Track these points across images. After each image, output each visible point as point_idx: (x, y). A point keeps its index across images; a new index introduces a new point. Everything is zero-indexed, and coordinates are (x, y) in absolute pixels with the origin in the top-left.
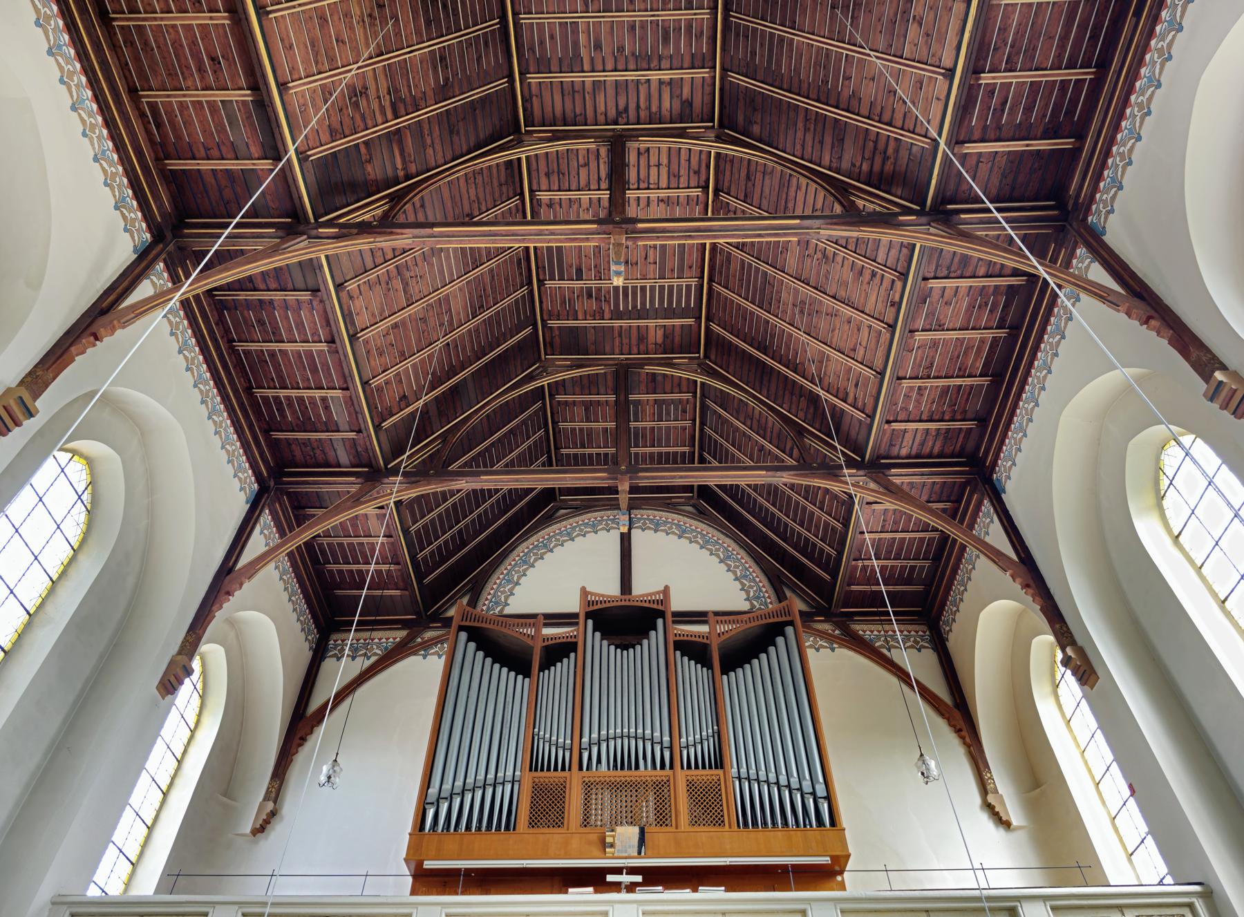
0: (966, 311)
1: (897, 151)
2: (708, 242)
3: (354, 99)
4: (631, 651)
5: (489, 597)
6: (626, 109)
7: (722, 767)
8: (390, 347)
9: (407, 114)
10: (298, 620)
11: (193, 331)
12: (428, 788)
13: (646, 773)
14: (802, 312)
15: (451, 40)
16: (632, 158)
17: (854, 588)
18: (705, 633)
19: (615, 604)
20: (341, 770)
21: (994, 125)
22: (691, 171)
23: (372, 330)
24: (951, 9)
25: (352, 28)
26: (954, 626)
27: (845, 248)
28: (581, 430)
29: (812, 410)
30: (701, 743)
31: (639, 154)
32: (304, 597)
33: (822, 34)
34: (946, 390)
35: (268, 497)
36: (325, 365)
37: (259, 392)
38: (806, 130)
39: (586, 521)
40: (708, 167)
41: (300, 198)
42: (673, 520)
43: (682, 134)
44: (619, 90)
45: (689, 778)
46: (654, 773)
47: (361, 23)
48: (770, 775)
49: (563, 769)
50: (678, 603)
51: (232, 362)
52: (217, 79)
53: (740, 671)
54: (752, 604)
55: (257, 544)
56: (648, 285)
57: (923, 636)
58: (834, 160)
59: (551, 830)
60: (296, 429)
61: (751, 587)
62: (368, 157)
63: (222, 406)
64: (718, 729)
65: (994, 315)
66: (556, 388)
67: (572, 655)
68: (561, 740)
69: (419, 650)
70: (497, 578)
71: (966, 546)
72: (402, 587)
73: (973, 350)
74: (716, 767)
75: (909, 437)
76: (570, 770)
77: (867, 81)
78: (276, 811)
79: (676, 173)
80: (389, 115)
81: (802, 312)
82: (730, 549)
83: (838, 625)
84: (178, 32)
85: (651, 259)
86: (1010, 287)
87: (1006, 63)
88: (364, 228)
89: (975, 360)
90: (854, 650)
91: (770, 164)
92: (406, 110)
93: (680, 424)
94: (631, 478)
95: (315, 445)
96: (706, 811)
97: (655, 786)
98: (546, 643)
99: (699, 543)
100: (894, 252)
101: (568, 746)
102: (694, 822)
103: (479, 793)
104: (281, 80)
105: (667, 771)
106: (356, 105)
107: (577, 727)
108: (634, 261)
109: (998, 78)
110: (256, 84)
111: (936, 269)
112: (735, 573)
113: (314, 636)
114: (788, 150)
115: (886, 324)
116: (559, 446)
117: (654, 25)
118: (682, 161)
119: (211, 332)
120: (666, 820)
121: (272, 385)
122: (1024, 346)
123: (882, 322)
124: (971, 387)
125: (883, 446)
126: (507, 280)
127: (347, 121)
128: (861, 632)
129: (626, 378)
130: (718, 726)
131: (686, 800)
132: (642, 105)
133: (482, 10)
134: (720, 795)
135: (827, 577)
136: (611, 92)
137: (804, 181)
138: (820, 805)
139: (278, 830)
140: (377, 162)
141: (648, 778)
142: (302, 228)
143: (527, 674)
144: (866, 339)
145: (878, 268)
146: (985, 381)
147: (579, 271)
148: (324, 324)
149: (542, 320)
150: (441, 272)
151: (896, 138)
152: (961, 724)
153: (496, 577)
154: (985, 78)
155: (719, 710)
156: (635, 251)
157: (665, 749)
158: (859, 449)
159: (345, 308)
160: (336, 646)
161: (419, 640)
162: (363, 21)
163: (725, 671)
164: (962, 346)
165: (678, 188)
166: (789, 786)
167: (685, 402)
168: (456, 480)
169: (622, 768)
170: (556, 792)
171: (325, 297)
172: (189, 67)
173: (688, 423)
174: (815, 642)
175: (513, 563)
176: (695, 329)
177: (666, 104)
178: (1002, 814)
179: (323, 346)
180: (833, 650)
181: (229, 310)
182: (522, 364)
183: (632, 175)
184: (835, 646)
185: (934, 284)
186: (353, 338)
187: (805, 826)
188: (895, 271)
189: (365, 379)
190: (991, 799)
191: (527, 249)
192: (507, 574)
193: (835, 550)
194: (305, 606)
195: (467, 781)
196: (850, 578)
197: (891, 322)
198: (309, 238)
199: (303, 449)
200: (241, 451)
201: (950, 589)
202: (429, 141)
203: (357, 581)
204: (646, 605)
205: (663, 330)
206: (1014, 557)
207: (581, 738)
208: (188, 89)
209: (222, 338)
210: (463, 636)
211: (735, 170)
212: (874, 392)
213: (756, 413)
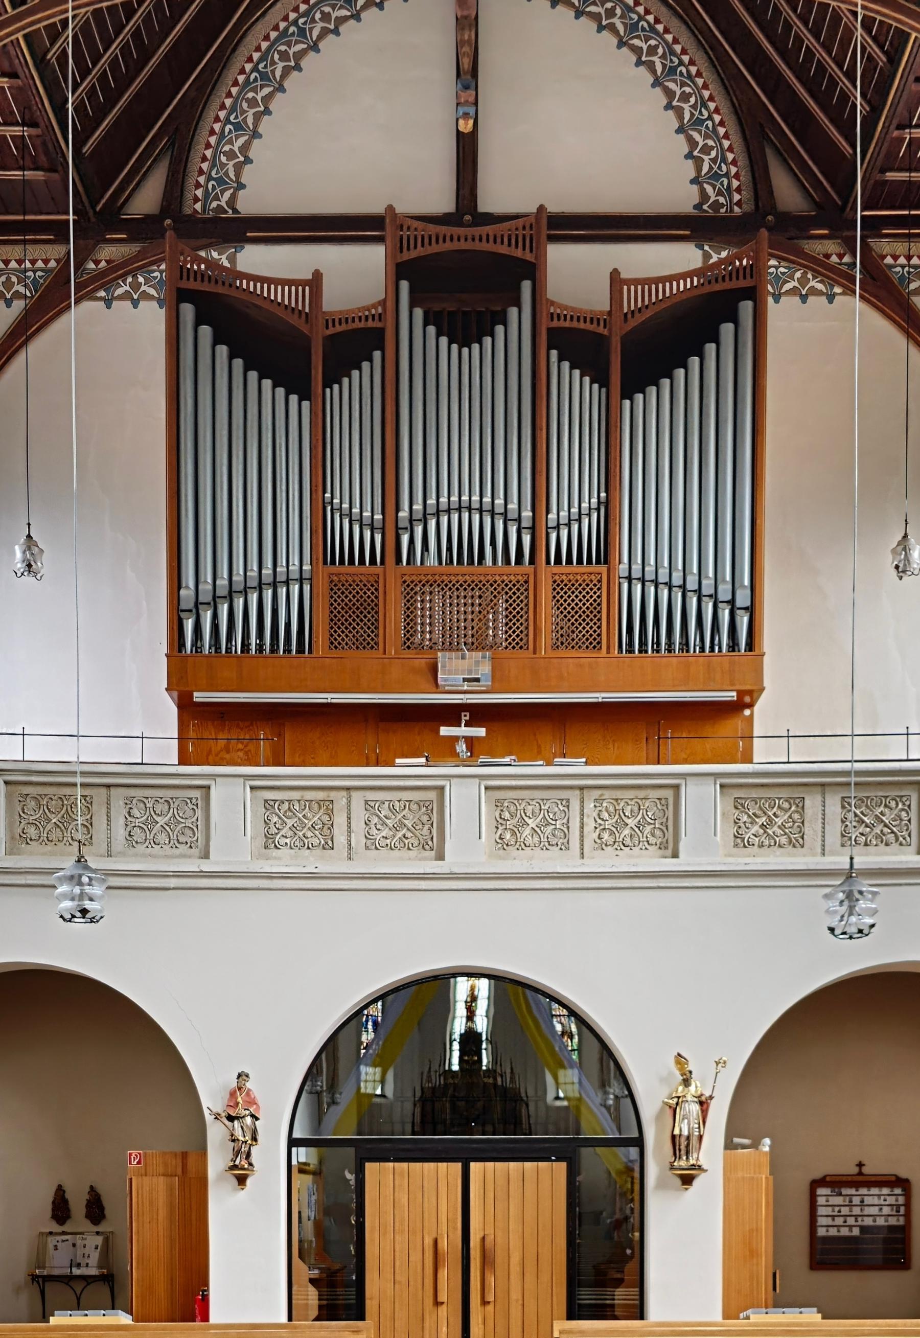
4: (476, 347)
7: (606, 562)
12: (179, 588)
17: (891, 176)
18: (602, 313)
20: (42, 551)
30: (579, 521)
45: (557, 577)
46: (507, 569)
64: (607, 496)
68: (367, 514)
74: (598, 562)
98: (331, 331)
130: (607, 491)
134: (599, 597)
138: (738, 619)
141: (497, 578)
153: (212, 115)
157: (524, 531)
163: (627, 394)
174: (803, 281)
180: (831, 298)
184: (837, 290)
192: (233, 109)
193: (884, 53)
196: (888, 155)
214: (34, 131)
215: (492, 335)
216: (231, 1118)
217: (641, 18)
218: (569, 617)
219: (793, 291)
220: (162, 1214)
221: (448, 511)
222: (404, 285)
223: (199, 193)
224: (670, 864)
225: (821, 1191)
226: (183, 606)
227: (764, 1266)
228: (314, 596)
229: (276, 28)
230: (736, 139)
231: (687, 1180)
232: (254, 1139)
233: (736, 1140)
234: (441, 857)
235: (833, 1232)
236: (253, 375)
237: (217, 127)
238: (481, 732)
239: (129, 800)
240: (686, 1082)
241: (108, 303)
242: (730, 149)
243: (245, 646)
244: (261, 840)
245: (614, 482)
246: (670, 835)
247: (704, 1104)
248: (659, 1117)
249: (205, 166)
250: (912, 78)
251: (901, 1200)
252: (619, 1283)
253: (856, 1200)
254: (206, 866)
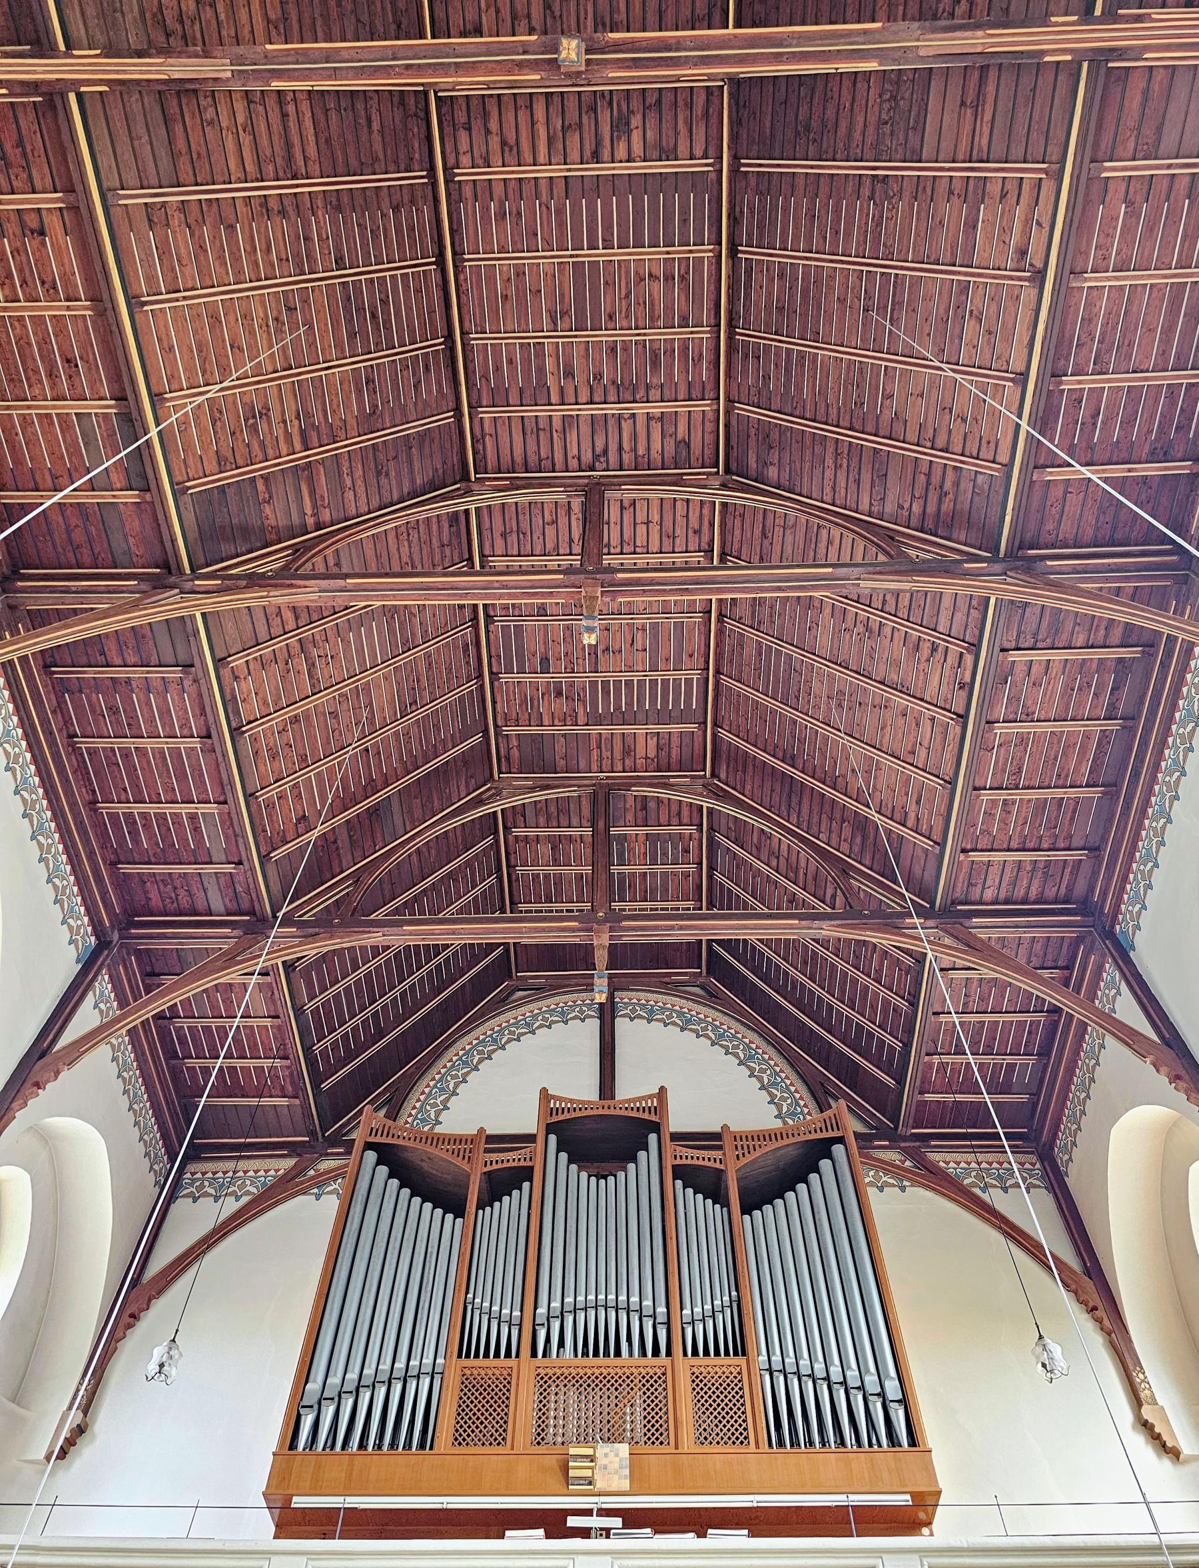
0: (1062, 695)
1: (957, 484)
2: (714, 598)
3: (251, 421)
4: (611, 1179)
5: (414, 1112)
6: (605, 452)
7: (744, 1354)
8: (287, 749)
9: (321, 446)
10: (141, 1139)
11: (21, 720)
12: (307, 1382)
13: (631, 1362)
14: (840, 706)
15: (382, 358)
16: (611, 512)
17: (929, 1097)
20: (181, 1355)
21: (1084, 445)
22: (690, 531)
23: (263, 723)
24: (1018, 297)
25: (252, 333)
26: (1076, 1153)
27: (895, 616)
28: (547, 876)
29: (858, 840)
31: (622, 508)
32: (152, 1106)
33: (853, 344)
34: (1041, 805)
35: (108, 956)
36: (196, 769)
38: (837, 467)
39: (553, 1007)
40: (712, 525)
41: (173, 541)
42: (673, 1006)
43: (678, 481)
44: (596, 426)
45: (695, 1369)
46: (643, 1362)
47: (264, 328)
48: (816, 1366)
49: (508, 1354)
50: (678, 1121)
51: (71, 766)
52: (72, 386)
53: (768, 1208)
54: (785, 1123)
55: (86, 1018)
56: (635, 679)
57: (1032, 1170)
58: (875, 503)
59: (487, 1450)
60: (153, 860)
61: (784, 1099)
62: (267, 496)
63: (53, 825)
65: (1101, 700)
66: (516, 815)
67: (526, 1185)
69: (311, 1187)
70: (424, 1086)
71: (1086, 1025)
72: (291, 1094)
73: (1075, 749)
75: (994, 872)
76: (517, 1356)
77: (914, 397)
78: (87, 1426)
79: (671, 534)
80: (298, 445)
81: (840, 706)
82: (754, 1046)
83: (909, 1153)
84: (25, 326)
85: (638, 645)
86: (1120, 660)
87: (1095, 364)
88: (255, 581)
89: (1079, 763)
90: (934, 1189)
91: (792, 514)
92: (319, 441)
93: (681, 868)
94: (611, 929)
95: (178, 883)
96: (720, 1422)
97: (644, 1381)
98: (489, 1168)
99: (709, 1038)
100: (960, 617)
101: (515, 1321)
102: (703, 1439)
103: (381, 1391)
104: (155, 390)
105: (663, 1359)
106: (254, 429)
107: (530, 1292)
108: (617, 648)
109: (1087, 383)
110: (123, 395)
111: (1018, 636)
112: (760, 1079)
114: (814, 496)
115: (954, 713)
116: (516, 899)
117: (640, 347)
118: (678, 518)
119: (44, 722)
120: (661, 1434)
121: (123, 798)
122: (1144, 742)
123: (950, 711)
124: (1077, 801)
125: (958, 890)
126: (449, 671)
127: (241, 451)
128: (942, 1164)
129: (607, 802)
130: (737, 1290)
131: (690, 1405)
132: (626, 446)
133: (422, 324)
135: (890, 1082)
136: (585, 429)
137: (836, 532)
139: (86, 1454)
140: (279, 504)
141: (634, 1370)
142: (172, 579)
143: (459, 1213)
144: (928, 736)
145: (939, 638)
146: (1095, 793)
147: (545, 660)
148: (198, 713)
149: (496, 726)
150: (360, 651)
151: (955, 468)
152: (1095, 1299)
154: (1068, 383)
155: (739, 1267)
156: (618, 635)
158: (925, 891)
159: (228, 691)
160: (194, 1181)
161: (312, 1172)
162: (267, 326)
163: (747, 1210)
164: (1059, 741)
165: (674, 552)
166: (844, 1383)
167: (687, 837)
168: (369, 932)
169: (596, 1354)
170: (497, 1390)
171: (200, 674)
172: (37, 372)
173: (692, 868)
175: (449, 1065)
176: (698, 740)
177: (656, 445)
178: (1165, 1437)
179: (196, 743)
180: (903, 1189)
181: (71, 693)
182: (467, 786)
183: (612, 535)
184: (905, 1183)
185: (1014, 656)
186: (235, 732)
187: (870, 1445)
188: (963, 641)
189: (250, 791)
190: (1147, 1413)
191: (475, 606)
192: (441, 1080)
194: (153, 1120)
195: (365, 1372)
197: (961, 711)
198: (182, 593)
199: (162, 886)
200: (75, 889)
201: (1066, 1097)
202: (348, 482)
203: (211, 1043)
205: (655, 739)
206: (1155, 1038)
207: (535, 1309)
208: (34, 398)
209: (60, 731)
210: (371, 1156)
211: (747, 526)
212: (943, 808)
213: (784, 848)
214: (287, 1063)
218: (711, 1409)
228: (444, 1389)
245: (743, 1282)
250: (930, 1013)
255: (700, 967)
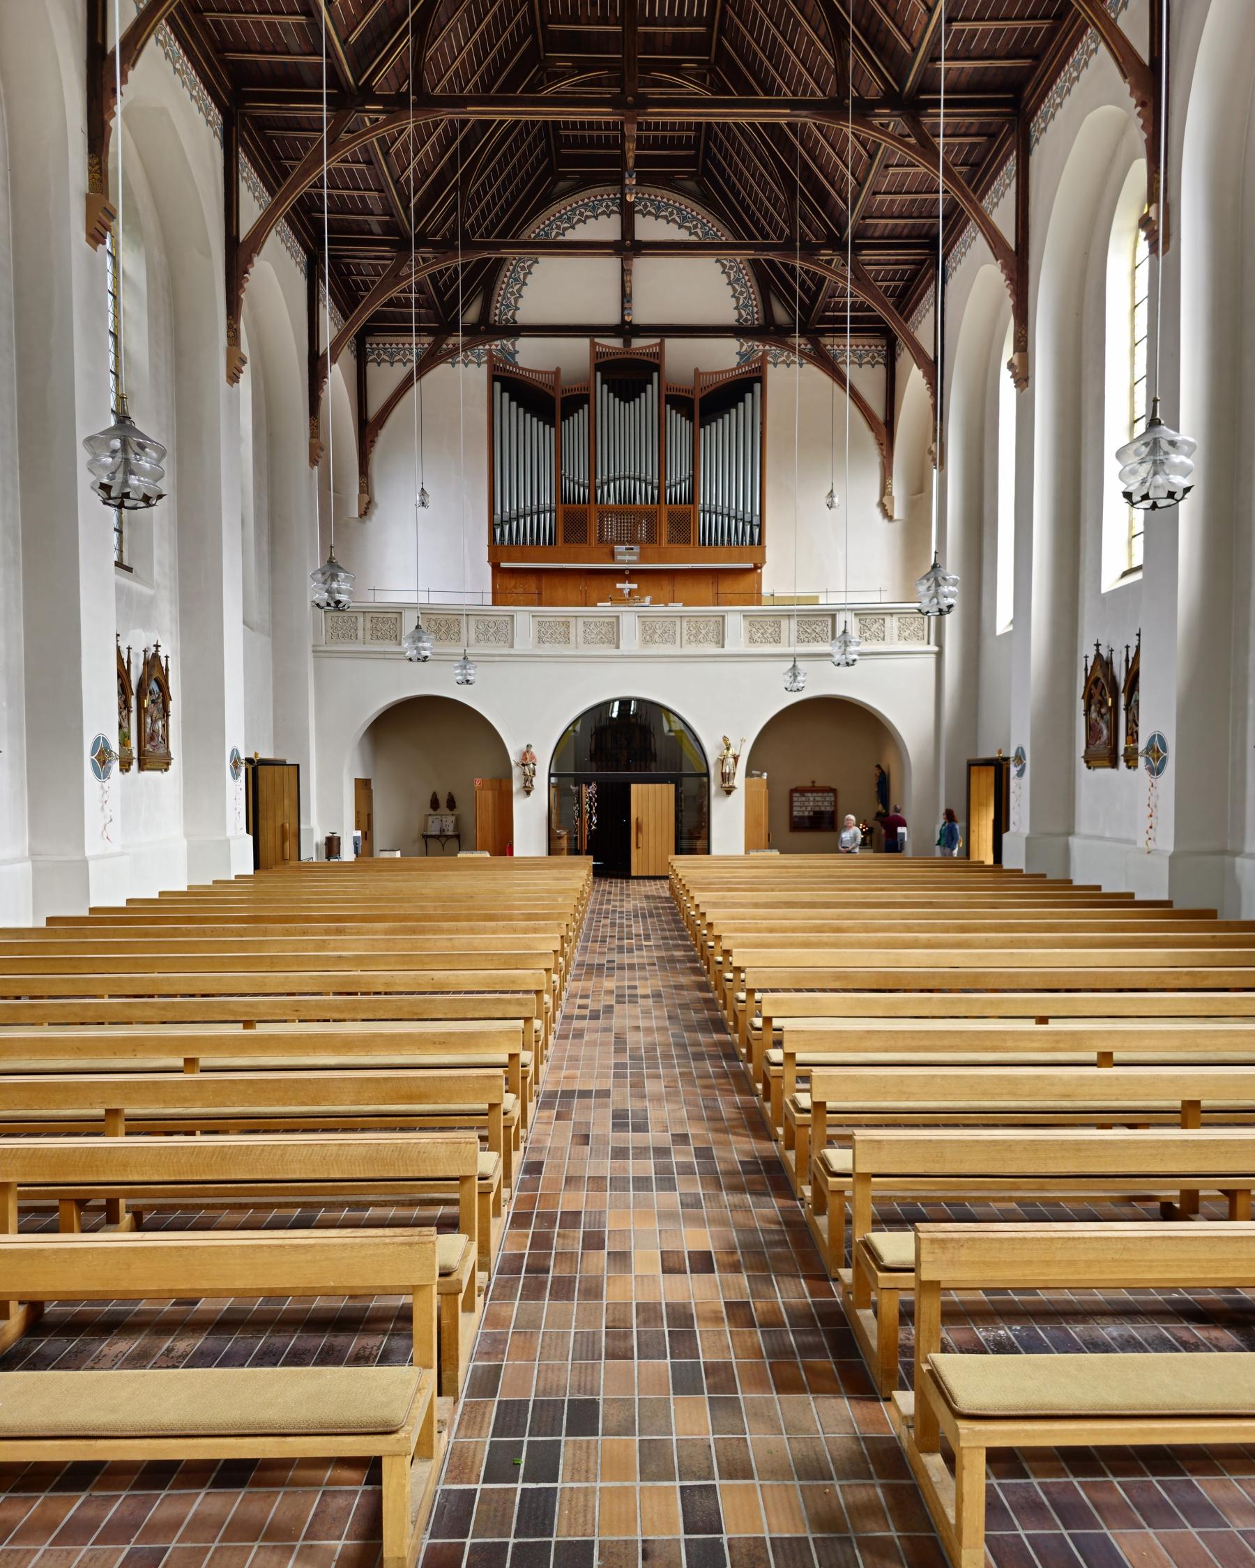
19: (619, 356)
37: (209, 16)
55: (251, 209)
98: (565, 395)
102: (669, 542)
113: (302, 257)
152: (884, 439)
163: (703, 425)
174: (788, 357)
184: (804, 361)
190: (885, 500)
192: (514, 271)
193: (867, 152)
204: (645, 358)
215: (640, 398)
216: (523, 765)
217: (710, 229)
219: (784, 362)
220: (490, 808)
221: (619, 479)
222: (599, 374)
223: (497, 312)
224: (720, 651)
225: (795, 795)
226: (496, 522)
227: (764, 830)
229: (534, 232)
230: (756, 288)
231: (729, 792)
232: (534, 774)
233: (754, 772)
234: (618, 647)
235: (801, 814)
236: (528, 416)
237: (506, 280)
238: (635, 586)
239: (477, 622)
240: (728, 749)
241: (453, 365)
242: (753, 293)
243: (525, 543)
244: (537, 640)
246: (721, 637)
247: (736, 758)
248: (716, 764)
249: (500, 299)
251: (833, 799)
252: (699, 838)
253: (811, 799)
254: (512, 652)
255: (709, 55)
